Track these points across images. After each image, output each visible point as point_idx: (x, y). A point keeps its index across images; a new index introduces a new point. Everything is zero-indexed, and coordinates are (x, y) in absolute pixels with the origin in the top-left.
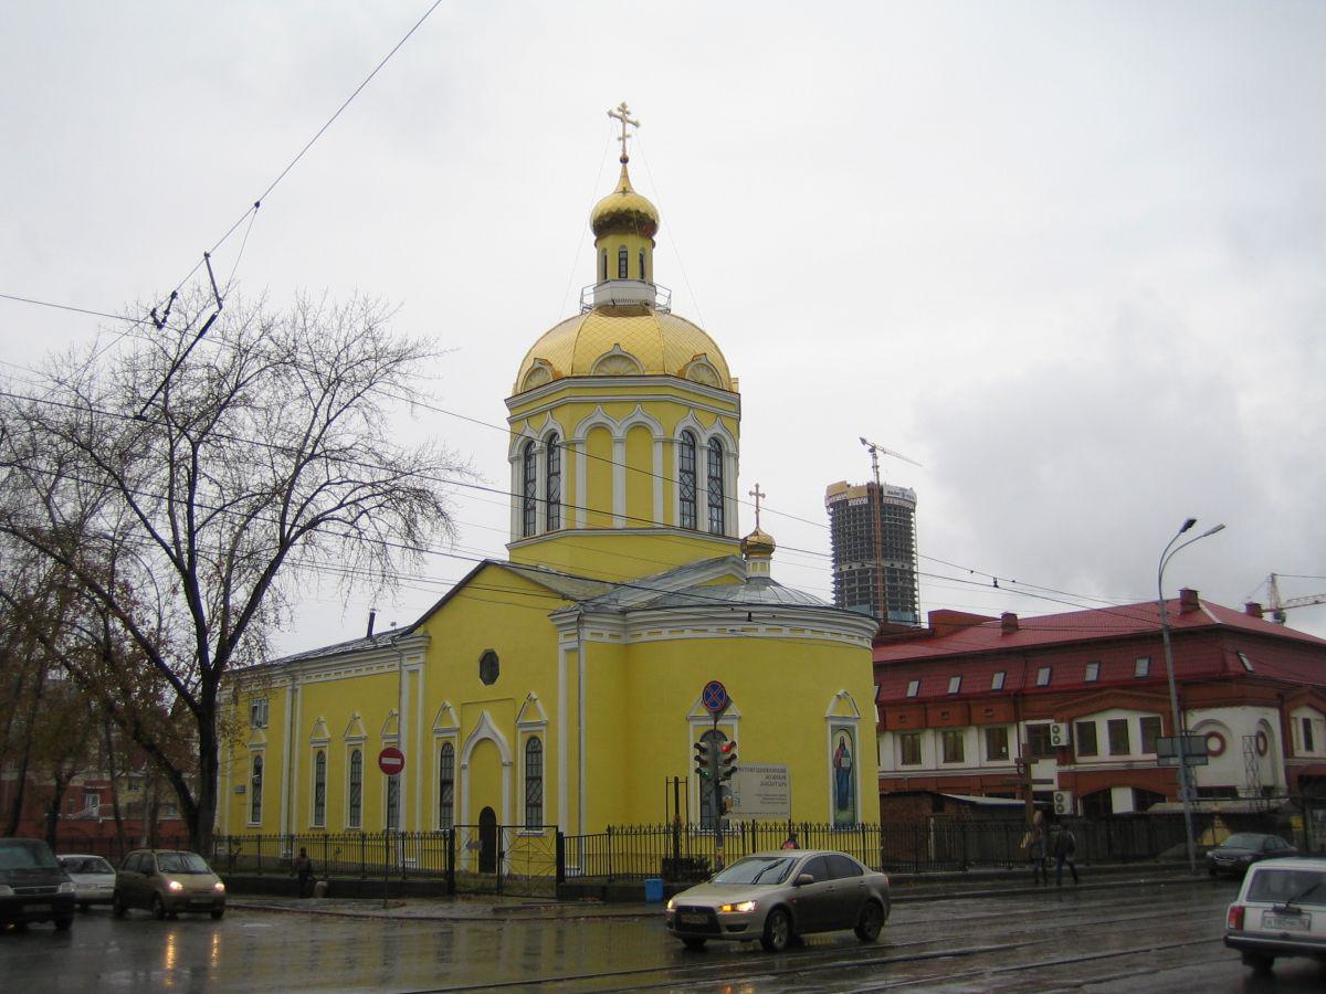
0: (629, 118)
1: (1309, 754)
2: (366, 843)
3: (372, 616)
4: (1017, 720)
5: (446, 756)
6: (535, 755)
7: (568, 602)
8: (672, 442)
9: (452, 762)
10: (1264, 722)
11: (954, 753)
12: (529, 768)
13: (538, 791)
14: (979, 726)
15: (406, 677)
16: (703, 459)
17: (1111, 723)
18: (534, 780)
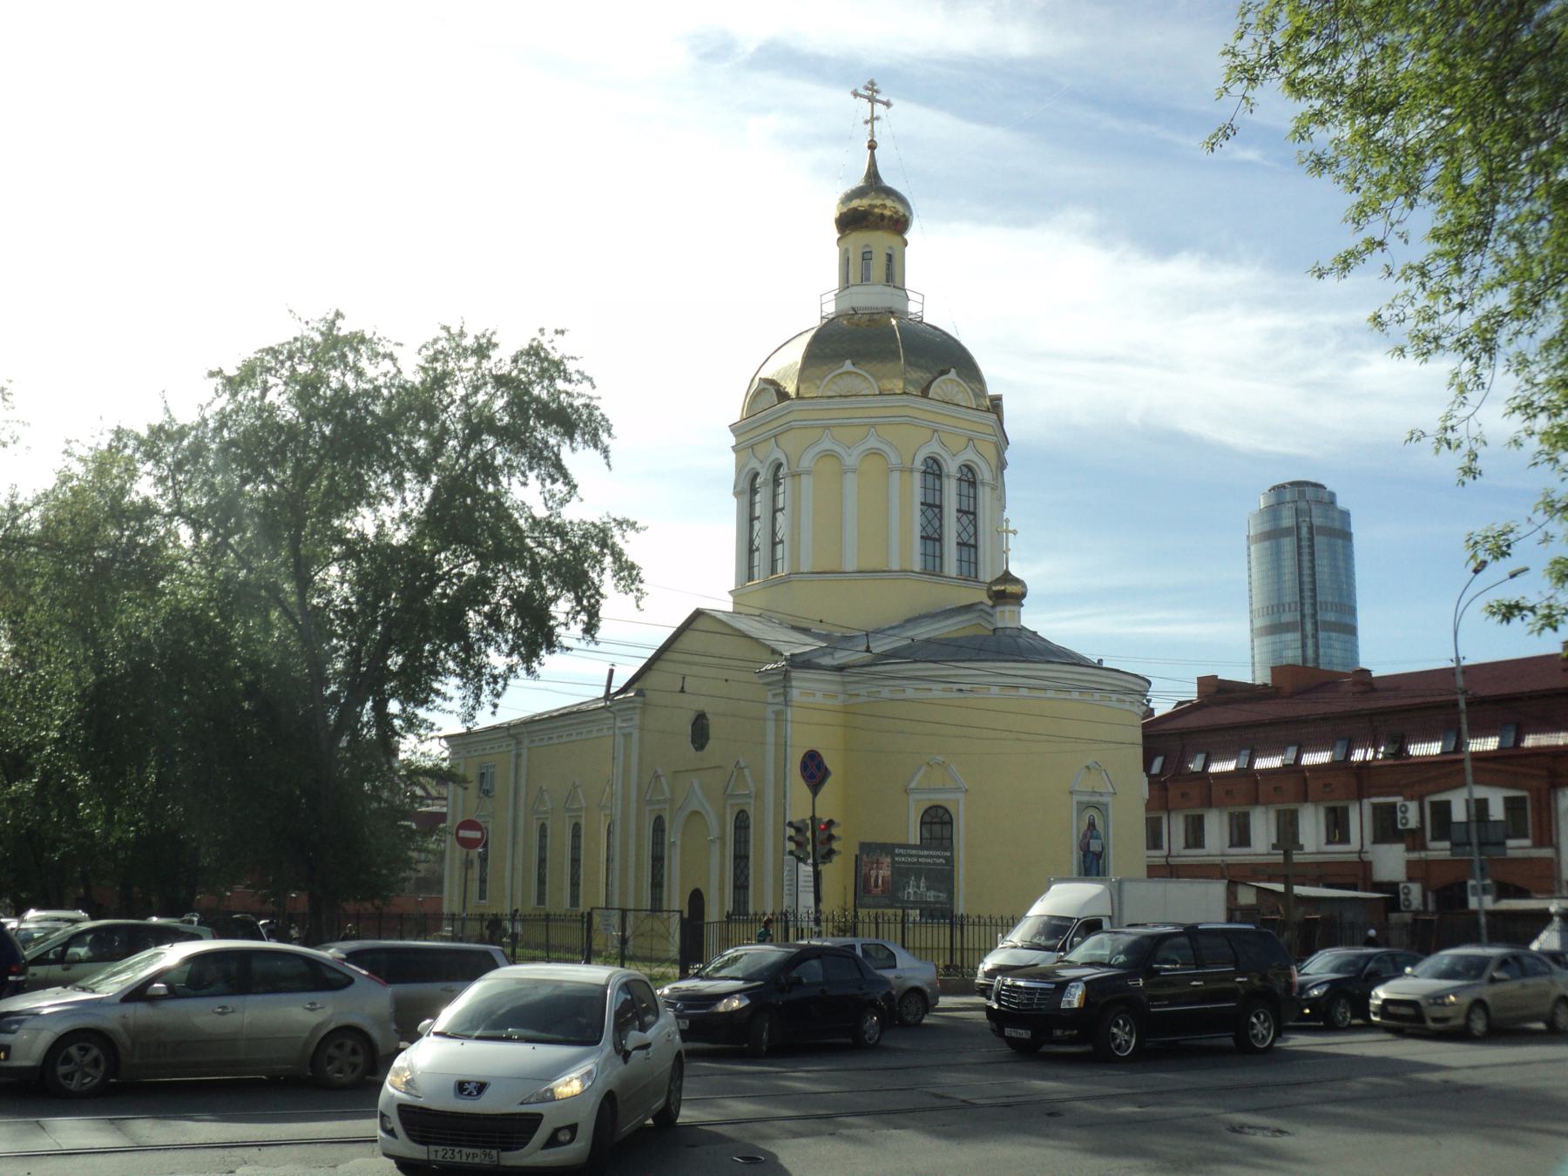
0: (878, 97)
3: (611, 672)
4: (1360, 797)
8: (911, 471)
14: (1316, 802)
16: (951, 489)
17: (1375, 807)
18: (741, 859)
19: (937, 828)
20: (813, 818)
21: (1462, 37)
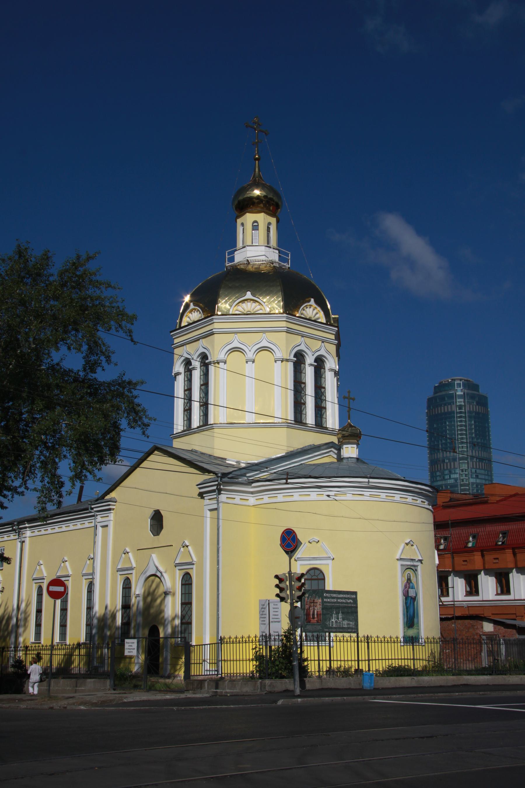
2: (54, 652)
6: (187, 586)
9: (130, 592)
11: (473, 588)
12: (183, 595)
13: (189, 613)
15: (100, 530)
20: (290, 572)
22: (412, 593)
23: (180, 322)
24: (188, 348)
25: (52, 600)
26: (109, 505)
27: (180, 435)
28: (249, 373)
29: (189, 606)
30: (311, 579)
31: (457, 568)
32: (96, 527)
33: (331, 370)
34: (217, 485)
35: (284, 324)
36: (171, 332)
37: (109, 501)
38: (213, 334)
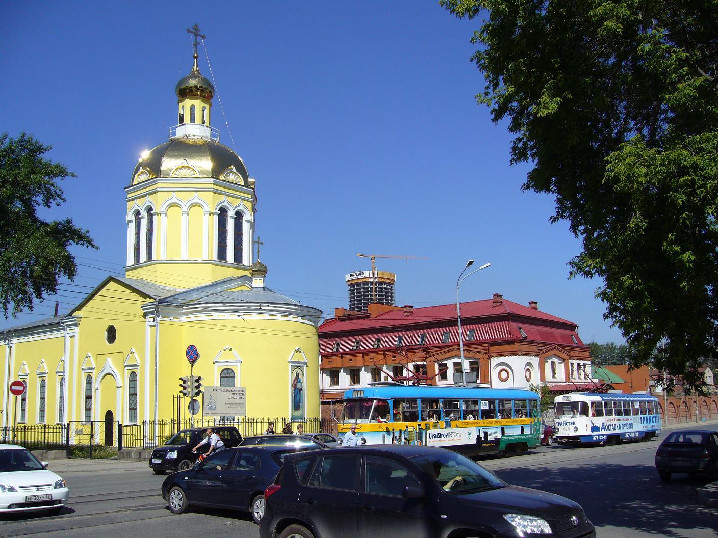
1: (554, 380)
2: (46, 430)
5: (132, 381)
6: (133, 382)
7: (148, 300)
9: (91, 386)
10: (529, 364)
15: (69, 339)
17: (455, 364)
19: (227, 379)
21: (714, 341)
22: (299, 385)
23: (133, 182)
24: (137, 201)
25: (15, 396)
26: (76, 321)
27: (132, 268)
28: (180, 223)
29: (135, 396)
30: (225, 377)
31: (345, 365)
32: (65, 336)
33: (247, 221)
34: (155, 308)
35: (212, 186)
36: (125, 188)
37: (75, 318)
38: (156, 192)
